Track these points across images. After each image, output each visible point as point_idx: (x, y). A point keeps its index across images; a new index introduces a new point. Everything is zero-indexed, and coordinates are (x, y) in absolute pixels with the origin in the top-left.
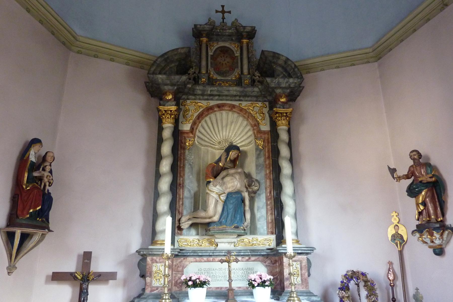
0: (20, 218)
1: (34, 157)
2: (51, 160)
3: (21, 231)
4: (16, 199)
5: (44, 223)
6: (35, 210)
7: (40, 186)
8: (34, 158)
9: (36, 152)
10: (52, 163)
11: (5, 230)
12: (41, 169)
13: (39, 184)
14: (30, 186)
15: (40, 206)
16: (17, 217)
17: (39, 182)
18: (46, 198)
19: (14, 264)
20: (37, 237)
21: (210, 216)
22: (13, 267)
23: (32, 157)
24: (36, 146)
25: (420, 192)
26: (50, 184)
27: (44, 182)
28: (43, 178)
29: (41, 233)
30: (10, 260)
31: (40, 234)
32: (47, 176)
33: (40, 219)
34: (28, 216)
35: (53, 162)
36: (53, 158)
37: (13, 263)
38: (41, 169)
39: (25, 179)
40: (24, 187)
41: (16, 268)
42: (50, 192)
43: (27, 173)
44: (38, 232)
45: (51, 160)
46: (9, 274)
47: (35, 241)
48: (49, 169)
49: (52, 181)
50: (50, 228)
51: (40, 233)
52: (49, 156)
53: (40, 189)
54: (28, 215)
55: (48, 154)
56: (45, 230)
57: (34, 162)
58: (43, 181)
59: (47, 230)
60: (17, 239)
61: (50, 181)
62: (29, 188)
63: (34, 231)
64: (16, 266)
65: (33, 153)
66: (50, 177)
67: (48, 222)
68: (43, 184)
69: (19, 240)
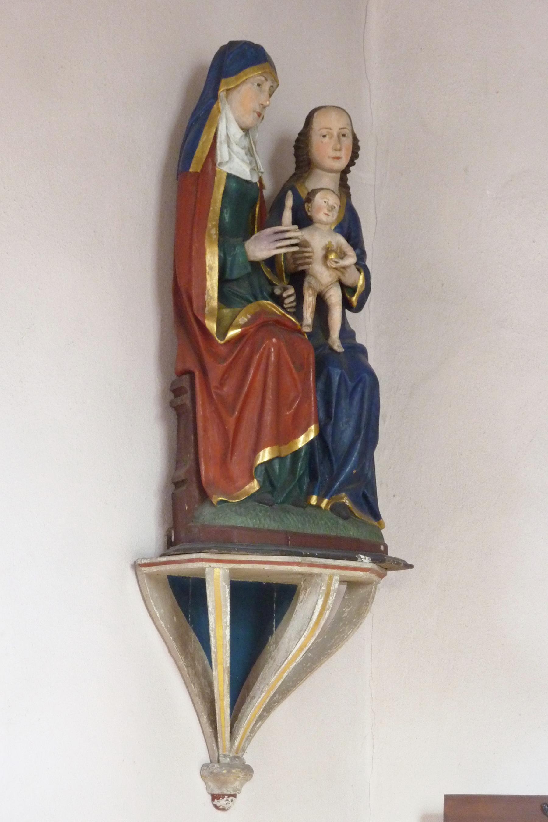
0: (216, 499)
1: (242, 152)
2: (338, 158)
3: (230, 570)
4: (186, 399)
5: (346, 518)
6: (286, 451)
7: (298, 313)
8: (243, 161)
9: (249, 120)
10: (348, 176)
11: (154, 569)
12: (287, 215)
13: (290, 301)
14: (242, 319)
15: (309, 425)
16: (204, 497)
17: (285, 295)
18: (336, 375)
19: (235, 748)
20: (320, 602)
21: (301, 597)
22: (230, 766)
23: (230, 158)
24: (245, 88)
25: (320, 585)
26: (354, 299)
27: (310, 287)
28: (309, 263)
29: (336, 578)
30: (209, 730)
31: (329, 585)
32: (328, 250)
33: (326, 501)
34: (255, 486)
35: (352, 162)
36: (348, 142)
37: (228, 743)
38: (287, 215)
39: (208, 283)
40: (212, 326)
41: (248, 771)
42: (360, 339)
43: (216, 249)
44: (315, 570)
45: (338, 158)
46: (216, 802)
47: (311, 619)
48: (333, 208)
49: (362, 277)
50: (386, 547)
51: (331, 578)
52: (324, 132)
53: (300, 332)
54: (251, 479)
55: (318, 123)
56: (355, 560)
57: (247, 182)
58: (306, 285)
59: (365, 561)
60: (219, 618)
61: (348, 280)
62: (238, 331)
63: (296, 568)
64: (248, 758)
65: (236, 133)
66: (342, 255)
67: (376, 516)
68: (310, 300)
69: (228, 618)
